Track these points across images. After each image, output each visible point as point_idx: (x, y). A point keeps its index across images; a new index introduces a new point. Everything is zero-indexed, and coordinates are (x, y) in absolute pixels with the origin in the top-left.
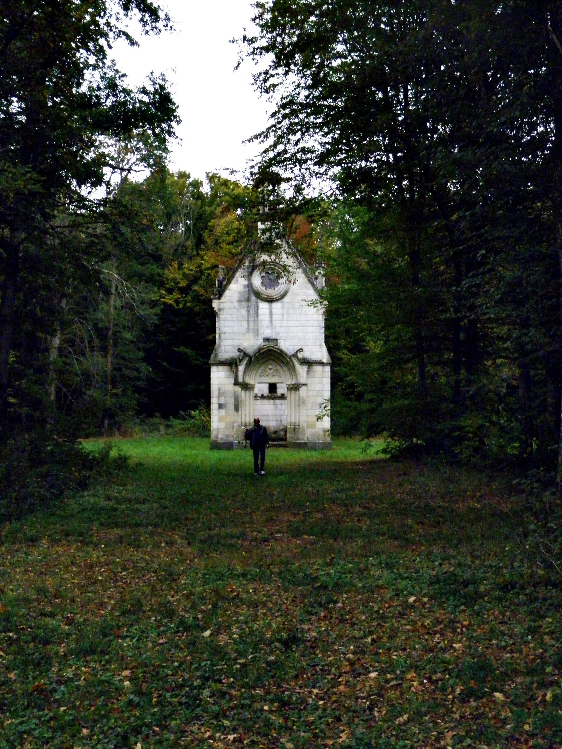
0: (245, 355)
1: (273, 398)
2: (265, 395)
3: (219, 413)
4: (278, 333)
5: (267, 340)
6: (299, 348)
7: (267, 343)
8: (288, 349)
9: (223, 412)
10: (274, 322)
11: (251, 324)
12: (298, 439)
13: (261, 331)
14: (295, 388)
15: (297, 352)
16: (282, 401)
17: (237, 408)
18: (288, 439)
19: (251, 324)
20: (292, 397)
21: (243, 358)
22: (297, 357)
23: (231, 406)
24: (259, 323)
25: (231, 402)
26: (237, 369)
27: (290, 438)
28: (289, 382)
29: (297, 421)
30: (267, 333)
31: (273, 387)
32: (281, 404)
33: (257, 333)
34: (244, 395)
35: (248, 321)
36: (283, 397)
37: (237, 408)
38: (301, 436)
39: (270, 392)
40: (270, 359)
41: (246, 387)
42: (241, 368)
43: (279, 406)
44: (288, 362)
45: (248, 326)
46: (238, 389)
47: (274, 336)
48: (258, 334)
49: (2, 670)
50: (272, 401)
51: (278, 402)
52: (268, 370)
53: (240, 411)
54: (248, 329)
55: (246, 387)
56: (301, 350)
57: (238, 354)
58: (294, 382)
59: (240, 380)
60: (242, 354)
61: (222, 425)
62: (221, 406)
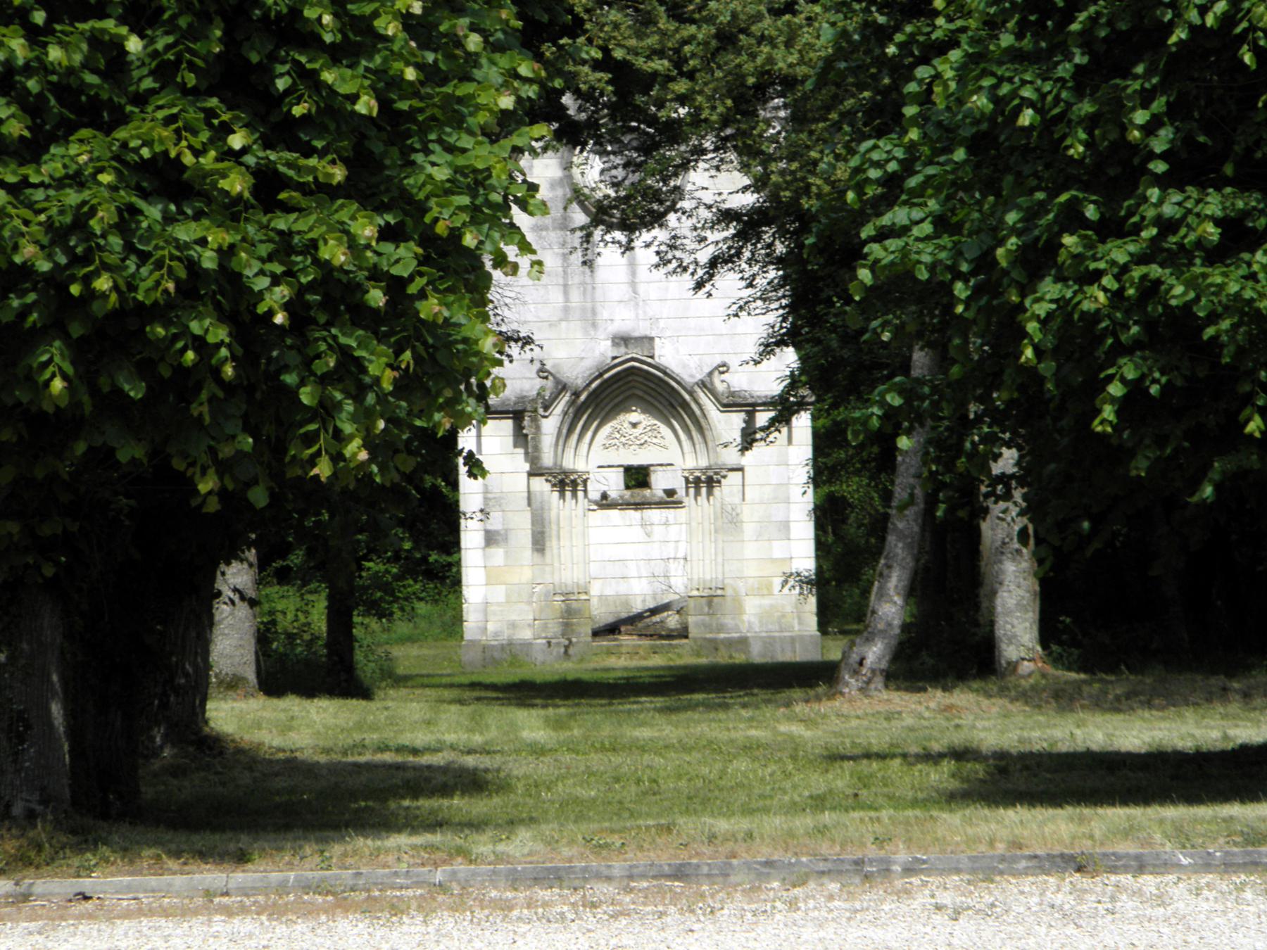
0: (562, 387)
1: (639, 505)
2: (613, 494)
3: (485, 557)
4: (654, 320)
5: (623, 340)
6: (718, 361)
7: (623, 350)
8: (685, 366)
9: (498, 554)
10: (642, 288)
11: (575, 296)
12: (721, 628)
13: (604, 314)
14: (706, 482)
15: (710, 374)
16: (670, 514)
17: (539, 543)
18: (693, 632)
19: (575, 296)
20: (697, 509)
21: (555, 397)
22: (712, 391)
23: (523, 537)
24: (599, 293)
25: (521, 524)
26: (538, 428)
27: (697, 624)
28: (690, 463)
29: (720, 577)
30: (623, 319)
31: (637, 477)
32: (666, 524)
33: (591, 320)
34: (563, 510)
35: (565, 286)
36: (670, 500)
37: (539, 543)
38: (728, 621)
39: (627, 487)
40: (634, 395)
41: (567, 483)
42: (550, 425)
43: (658, 531)
44: (685, 406)
45: (567, 300)
46: (540, 485)
47: (641, 330)
48: (594, 325)
49: (7, 435)
50: (634, 515)
51: (654, 515)
52: (1127, 904)
53: (548, 552)
54: (566, 310)
55: (567, 483)
56: (723, 368)
57: (538, 383)
58: (703, 463)
59: (547, 459)
60: (549, 383)
61: (498, 594)
62: (491, 539)
